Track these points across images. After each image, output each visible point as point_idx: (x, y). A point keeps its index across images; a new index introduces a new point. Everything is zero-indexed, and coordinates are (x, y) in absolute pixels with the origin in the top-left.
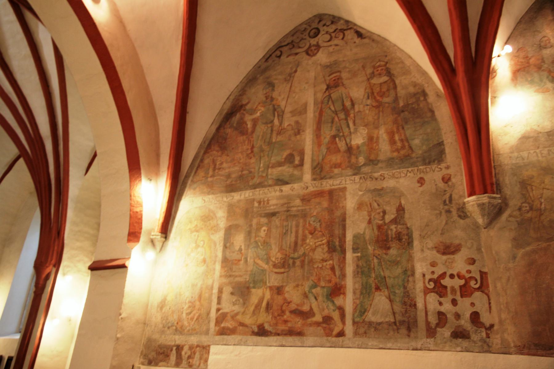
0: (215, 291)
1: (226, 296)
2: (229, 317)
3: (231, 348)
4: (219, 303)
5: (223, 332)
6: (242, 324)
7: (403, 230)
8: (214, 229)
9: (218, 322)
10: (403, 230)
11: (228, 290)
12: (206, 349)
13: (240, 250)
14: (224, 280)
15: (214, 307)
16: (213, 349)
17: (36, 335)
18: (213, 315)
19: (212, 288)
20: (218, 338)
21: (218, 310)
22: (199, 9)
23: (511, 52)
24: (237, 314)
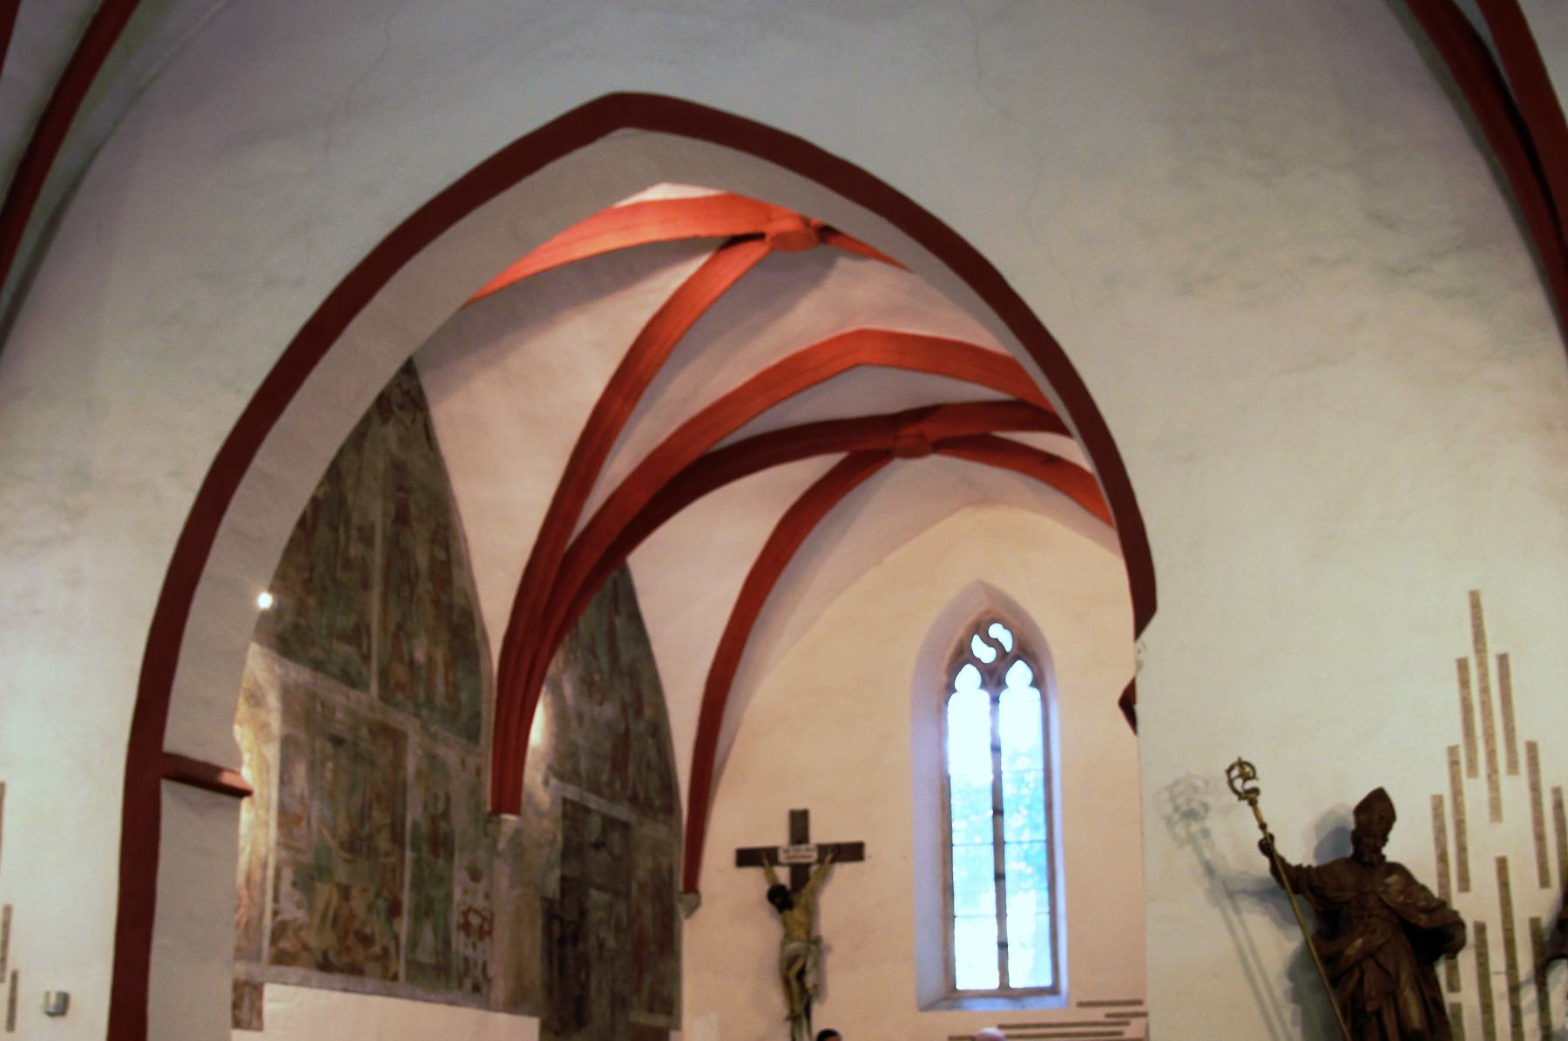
0: (270, 873)
1: (286, 887)
2: (290, 933)
3: (291, 990)
4: (276, 899)
5: (281, 958)
6: (306, 947)
7: (385, 893)
8: (268, 739)
9: (276, 936)
10: (385, 893)
11: (288, 874)
12: (258, 989)
13: (302, 797)
14: (284, 854)
15: (269, 907)
16: (270, 990)
17: (546, 708)
18: (268, 922)
19: (265, 866)
20: (274, 970)
21: (275, 913)
22: (740, 669)
23: (1003, 838)
24: (300, 928)
